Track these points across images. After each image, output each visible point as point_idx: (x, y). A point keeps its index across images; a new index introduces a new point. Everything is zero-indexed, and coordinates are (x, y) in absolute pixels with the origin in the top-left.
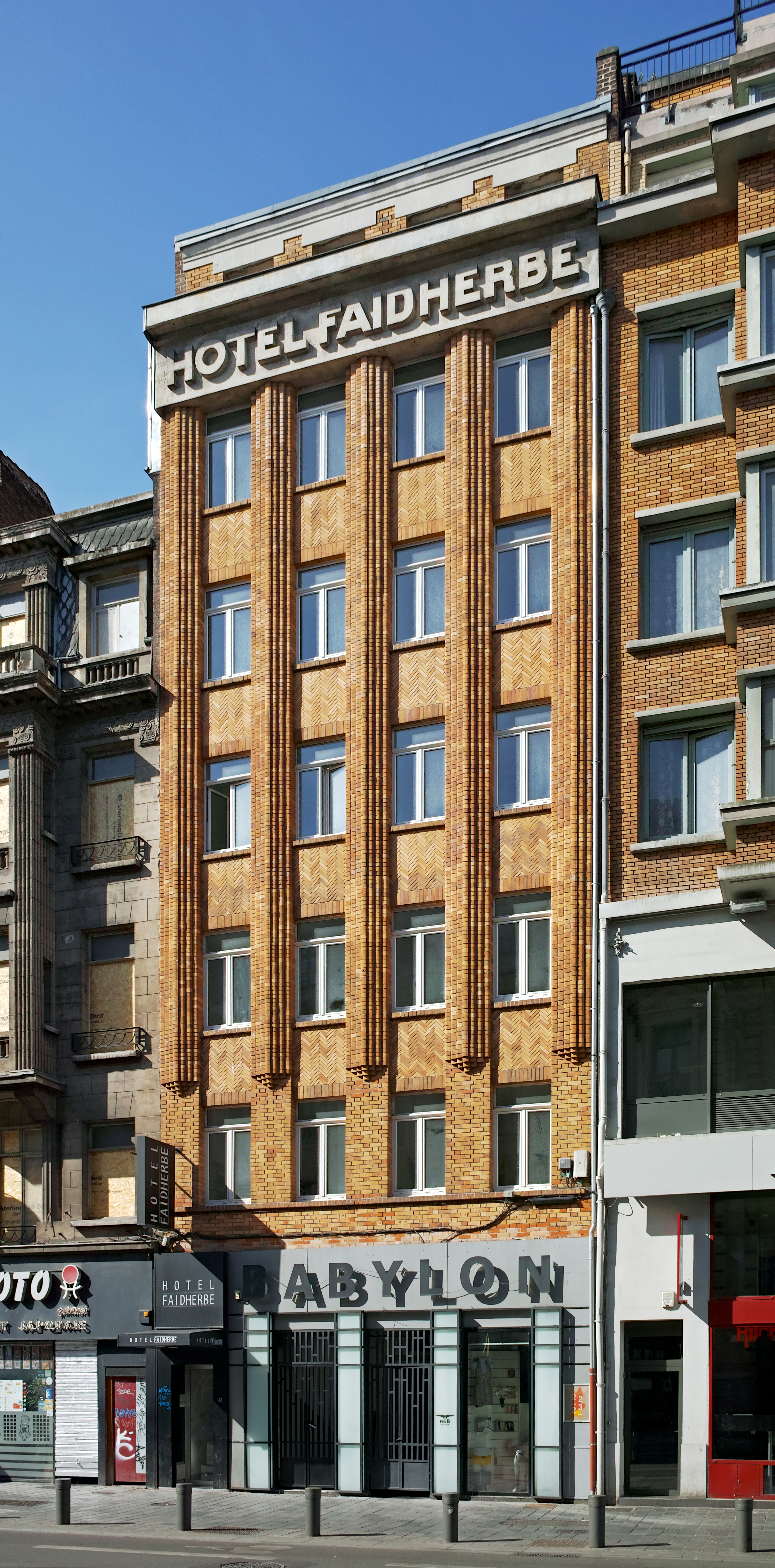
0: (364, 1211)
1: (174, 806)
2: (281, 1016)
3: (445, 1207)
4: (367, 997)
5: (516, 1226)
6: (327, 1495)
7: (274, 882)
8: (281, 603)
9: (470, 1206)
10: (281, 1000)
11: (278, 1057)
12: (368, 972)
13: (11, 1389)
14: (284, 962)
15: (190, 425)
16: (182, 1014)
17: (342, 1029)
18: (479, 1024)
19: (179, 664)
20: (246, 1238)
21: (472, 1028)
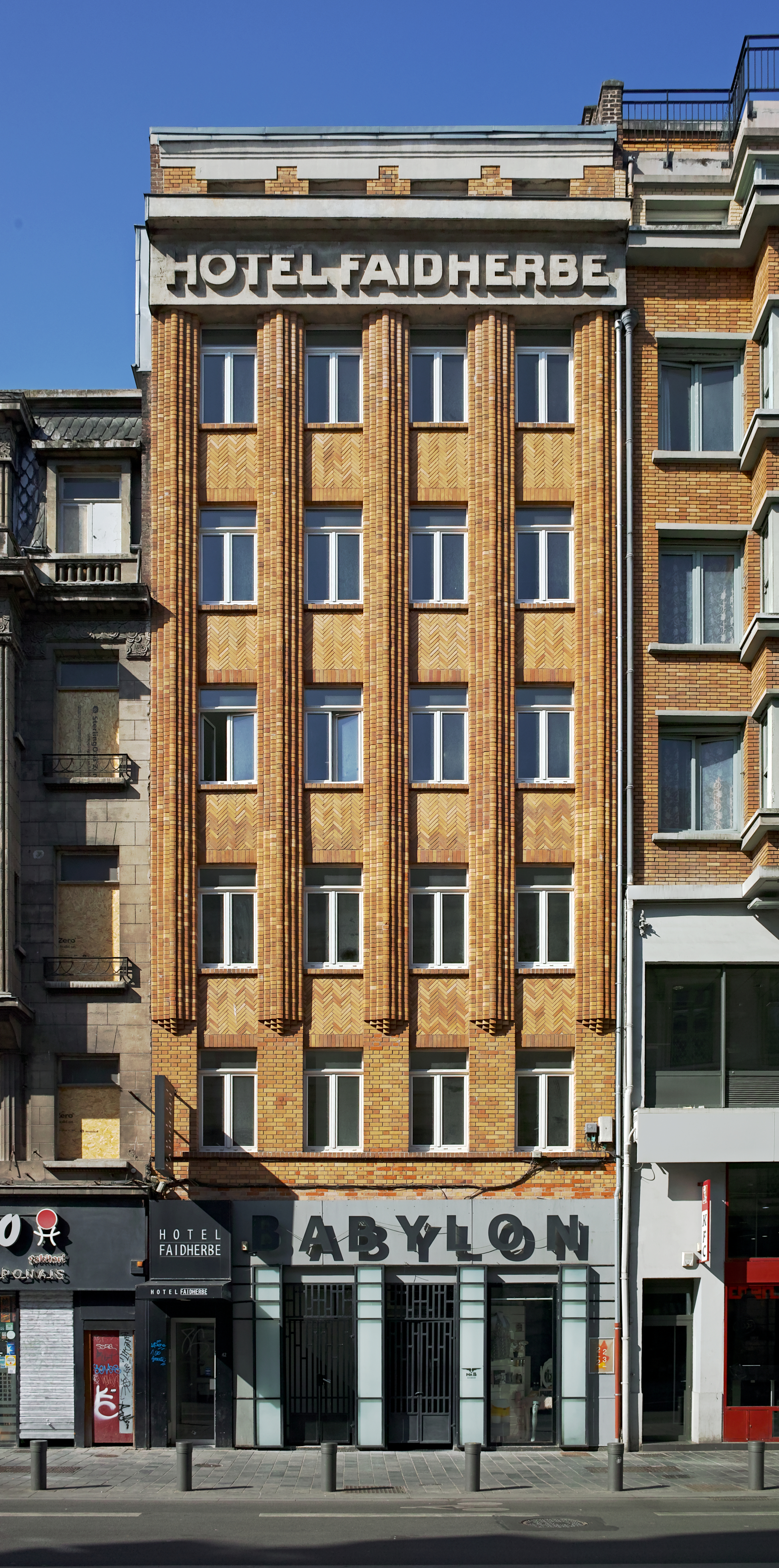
0: (384, 1165)
1: (171, 728)
2: (293, 961)
3: (469, 1164)
4: (390, 951)
5: (541, 1185)
6: (343, 1450)
7: (287, 823)
8: (293, 538)
9: (494, 1164)
10: (293, 944)
11: (290, 1003)
12: (390, 926)
14: (297, 906)
15: (188, 331)
16: (180, 948)
17: (358, 981)
18: (506, 988)
19: (177, 580)
20: (252, 1187)
21: (500, 991)
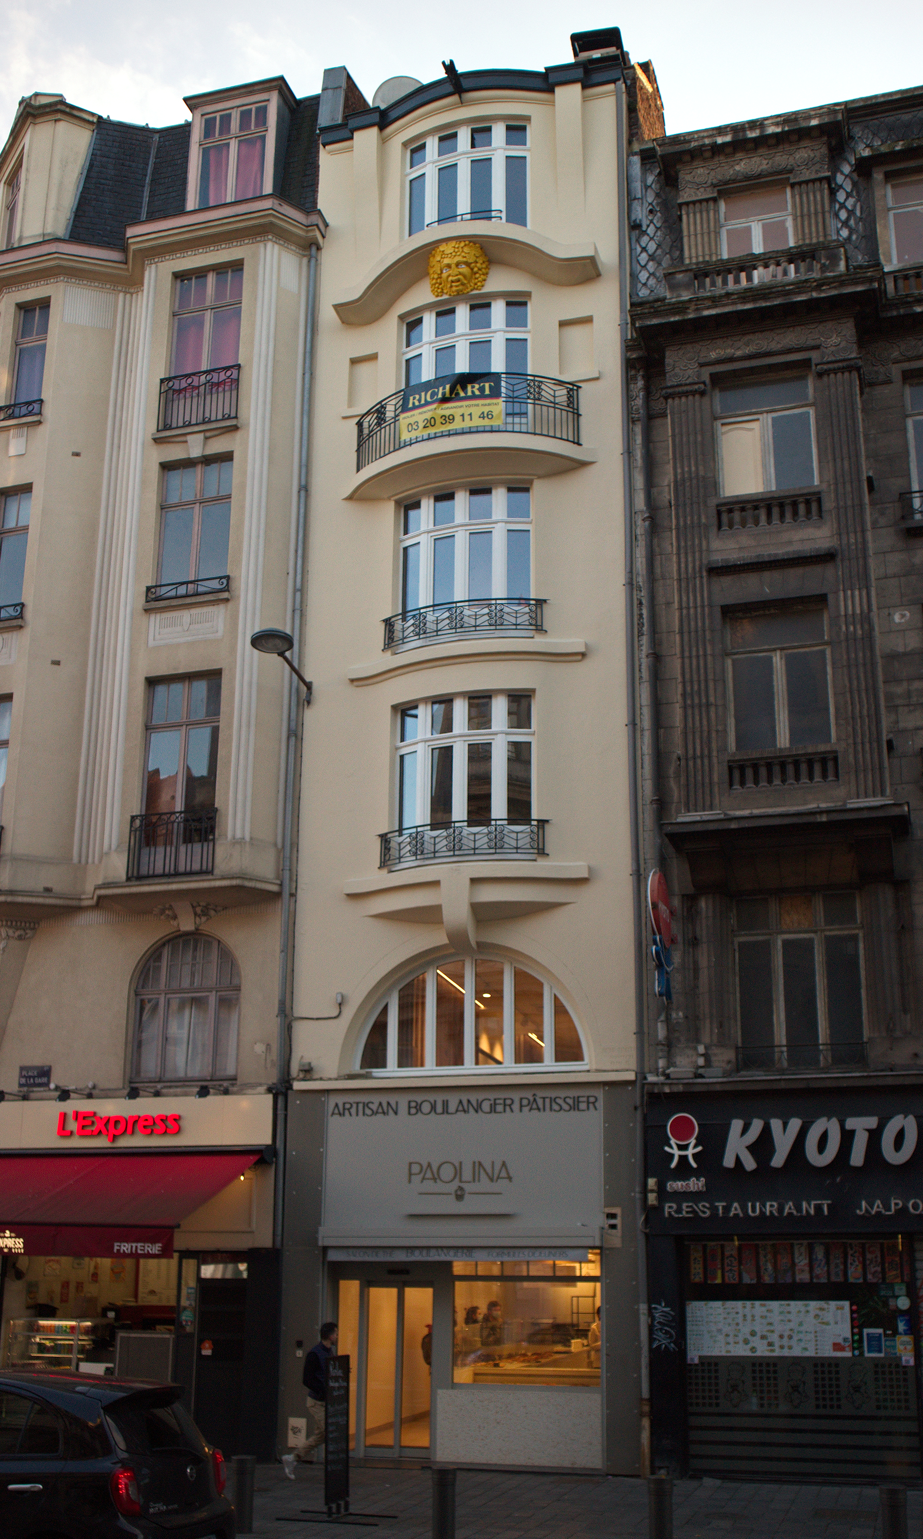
13: (829, 1317)
